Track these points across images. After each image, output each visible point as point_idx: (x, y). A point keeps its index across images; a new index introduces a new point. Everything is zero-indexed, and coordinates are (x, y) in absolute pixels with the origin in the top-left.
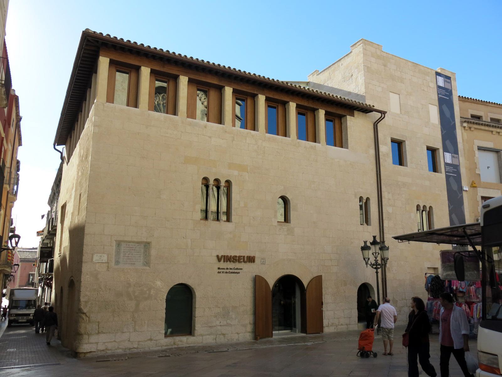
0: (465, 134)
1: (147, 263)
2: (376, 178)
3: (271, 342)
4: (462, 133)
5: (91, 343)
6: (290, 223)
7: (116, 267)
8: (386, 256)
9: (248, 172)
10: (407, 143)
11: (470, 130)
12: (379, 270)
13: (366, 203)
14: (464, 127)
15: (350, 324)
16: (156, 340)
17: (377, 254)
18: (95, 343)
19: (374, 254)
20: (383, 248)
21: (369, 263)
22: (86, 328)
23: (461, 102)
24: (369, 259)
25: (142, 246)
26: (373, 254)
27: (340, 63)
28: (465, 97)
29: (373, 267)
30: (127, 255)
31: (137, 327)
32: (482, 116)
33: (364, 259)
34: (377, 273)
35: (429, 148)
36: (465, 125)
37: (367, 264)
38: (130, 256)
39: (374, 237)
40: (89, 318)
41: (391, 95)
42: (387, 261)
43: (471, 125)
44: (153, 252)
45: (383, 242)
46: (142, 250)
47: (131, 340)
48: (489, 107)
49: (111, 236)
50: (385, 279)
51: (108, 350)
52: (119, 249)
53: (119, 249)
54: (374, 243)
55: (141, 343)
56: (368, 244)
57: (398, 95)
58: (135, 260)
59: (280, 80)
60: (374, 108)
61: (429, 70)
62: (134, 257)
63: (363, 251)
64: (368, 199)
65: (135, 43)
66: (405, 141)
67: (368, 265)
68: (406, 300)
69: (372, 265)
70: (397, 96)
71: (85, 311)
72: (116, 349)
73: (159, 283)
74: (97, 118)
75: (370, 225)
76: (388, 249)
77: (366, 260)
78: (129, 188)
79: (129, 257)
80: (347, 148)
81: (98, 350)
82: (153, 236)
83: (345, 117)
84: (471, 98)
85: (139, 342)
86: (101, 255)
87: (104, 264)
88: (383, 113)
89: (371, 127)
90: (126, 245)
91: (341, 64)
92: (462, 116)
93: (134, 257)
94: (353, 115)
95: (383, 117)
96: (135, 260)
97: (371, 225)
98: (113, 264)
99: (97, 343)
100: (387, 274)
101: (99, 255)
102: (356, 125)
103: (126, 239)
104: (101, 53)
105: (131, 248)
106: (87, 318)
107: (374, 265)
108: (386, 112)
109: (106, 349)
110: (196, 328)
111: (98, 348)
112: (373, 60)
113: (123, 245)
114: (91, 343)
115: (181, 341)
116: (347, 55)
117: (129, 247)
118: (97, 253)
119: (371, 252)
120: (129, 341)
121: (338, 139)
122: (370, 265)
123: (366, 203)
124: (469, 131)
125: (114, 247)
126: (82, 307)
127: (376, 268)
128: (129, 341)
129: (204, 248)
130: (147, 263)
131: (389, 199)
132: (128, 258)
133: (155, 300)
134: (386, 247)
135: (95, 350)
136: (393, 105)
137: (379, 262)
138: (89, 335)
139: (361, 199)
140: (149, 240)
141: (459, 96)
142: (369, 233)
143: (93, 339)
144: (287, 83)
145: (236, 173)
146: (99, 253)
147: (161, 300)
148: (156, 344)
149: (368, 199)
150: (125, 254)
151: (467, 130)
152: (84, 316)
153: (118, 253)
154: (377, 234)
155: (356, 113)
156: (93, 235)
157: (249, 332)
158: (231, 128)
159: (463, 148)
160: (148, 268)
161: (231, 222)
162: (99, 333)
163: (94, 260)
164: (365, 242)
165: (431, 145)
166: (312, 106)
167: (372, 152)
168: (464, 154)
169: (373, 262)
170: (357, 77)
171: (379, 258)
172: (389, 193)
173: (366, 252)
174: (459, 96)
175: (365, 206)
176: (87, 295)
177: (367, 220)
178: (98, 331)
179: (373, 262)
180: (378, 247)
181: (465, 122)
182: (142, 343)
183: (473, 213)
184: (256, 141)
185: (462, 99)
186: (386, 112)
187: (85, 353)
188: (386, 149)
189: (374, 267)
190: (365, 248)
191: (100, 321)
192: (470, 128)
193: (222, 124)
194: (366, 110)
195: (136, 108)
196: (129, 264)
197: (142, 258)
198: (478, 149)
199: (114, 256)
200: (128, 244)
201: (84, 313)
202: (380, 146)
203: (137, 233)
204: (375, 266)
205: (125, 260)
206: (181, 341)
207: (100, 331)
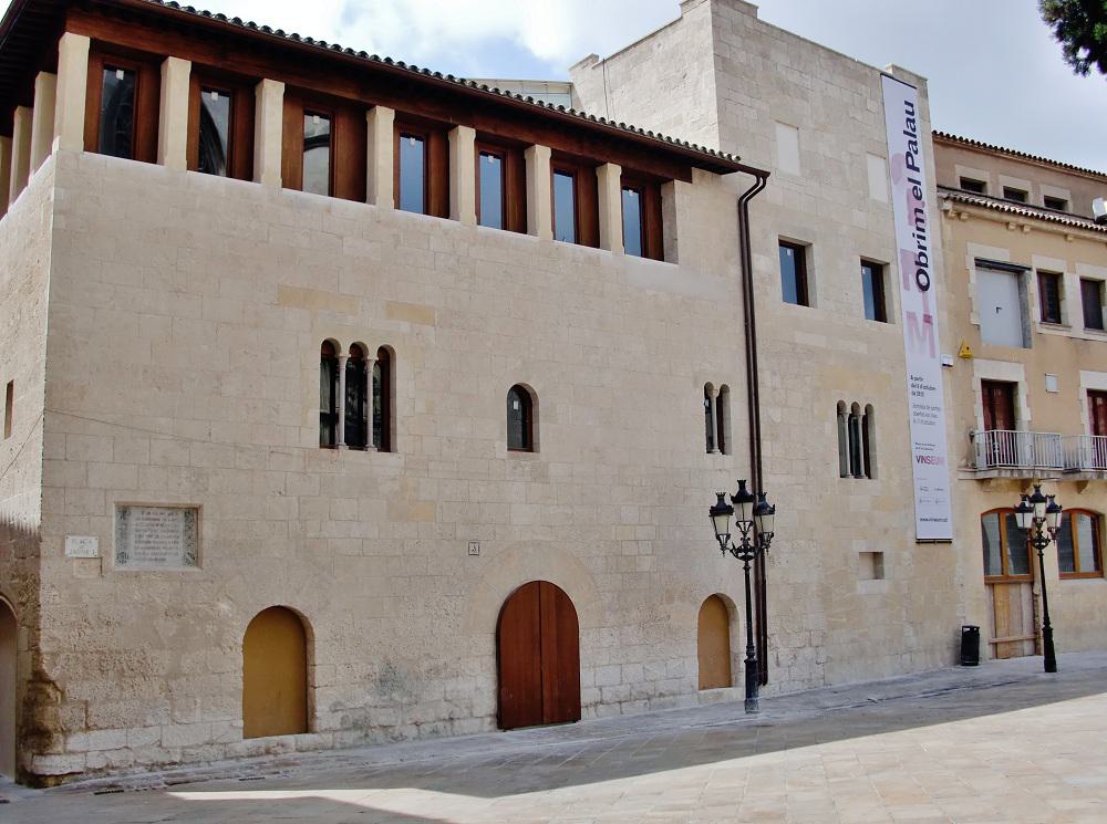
0: (948, 227)
1: (194, 558)
2: (743, 336)
3: (578, 734)
4: (941, 225)
5: (73, 753)
6: (539, 452)
7: (123, 568)
8: (768, 528)
9: (434, 325)
10: (815, 247)
11: (959, 218)
12: (751, 563)
13: (720, 400)
14: (946, 212)
15: (680, 694)
16: (225, 744)
17: (747, 524)
18: (82, 752)
19: (741, 524)
20: (762, 509)
21: (730, 546)
22: (56, 717)
23: (939, 147)
24: (728, 536)
25: (181, 515)
26: (737, 524)
27: (654, 43)
28: (948, 135)
29: (737, 557)
30: (145, 539)
31: (177, 713)
32: (985, 183)
33: (718, 537)
34: (747, 568)
35: (865, 263)
36: (948, 205)
37: (723, 548)
38: (151, 539)
39: (742, 484)
40: (63, 693)
41: (780, 129)
42: (769, 541)
43: (960, 208)
44: (207, 529)
45: (762, 496)
46: (182, 526)
47: (164, 745)
48: (1001, 160)
49: (106, 490)
50: (764, 582)
51: (113, 768)
52: (126, 525)
53: (126, 525)
54: (741, 498)
55: (188, 750)
56: (728, 501)
57: (795, 131)
58: (164, 551)
59: (458, 76)
60: (740, 162)
61: (867, 70)
62: (162, 542)
63: (716, 518)
64: (724, 389)
65: (222, 16)
66: (811, 244)
67: (727, 552)
68: (810, 631)
69: (736, 551)
70: (792, 133)
71: (53, 674)
72: (130, 766)
73: (224, 606)
74: (62, 191)
75: (730, 454)
76: (772, 511)
77: (722, 540)
78: (145, 371)
79: (149, 542)
80: (674, 261)
81: (89, 769)
82: (207, 489)
83: (669, 184)
84: (961, 138)
85: (183, 748)
86: (82, 538)
87: (93, 562)
88: (762, 175)
89: (733, 208)
90: (143, 513)
91: (656, 44)
92: (940, 184)
93: (162, 542)
94: (689, 179)
95: (761, 185)
96: (164, 551)
97: (730, 454)
98: (112, 561)
99: (85, 753)
100: (768, 572)
101: (79, 538)
102: (694, 207)
103: (142, 498)
104: (70, 23)
105: (155, 519)
106: (58, 693)
107: (739, 550)
108: (768, 174)
109: (107, 766)
110: (318, 714)
111: (88, 765)
112: (736, 41)
113: (135, 515)
114: (73, 753)
115: (283, 746)
116: (671, 25)
117: (147, 519)
118: (74, 534)
119: (733, 519)
120: (160, 746)
121: (653, 242)
122: (731, 551)
123: (720, 400)
124: (957, 222)
125: (114, 520)
126: (44, 667)
127: (746, 558)
128: (160, 746)
129: (330, 519)
130: (194, 558)
131: (775, 389)
132: (148, 545)
133: (218, 649)
134: (768, 506)
135: (81, 770)
136: (783, 154)
137: (751, 543)
138: (66, 732)
139: (708, 389)
140: (196, 502)
141: (935, 132)
142: (729, 472)
143: (76, 741)
144: (463, 80)
145: (405, 327)
146: (79, 534)
147: (231, 648)
148: (225, 753)
149: (724, 389)
150: (140, 536)
151: (952, 218)
152: (50, 690)
153: (123, 534)
154: (746, 475)
155: (696, 172)
156: (63, 491)
157: (490, 715)
158: (469, 228)
159: (942, 260)
160: (196, 569)
161: (396, 451)
162: (88, 728)
163: (67, 552)
164: (721, 497)
165: (794, 236)
166: (590, 155)
167: (735, 271)
168: (945, 276)
169: (739, 544)
170: (698, 82)
171: (750, 535)
172: (775, 374)
173: (721, 520)
174: (935, 132)
175: (716, 405)
176: (54, 639)
177: (717, 439)
178: (86, 724)
179: (739, 544)
180: (749, 507)
181: (947, 198)
182: (192, 751)
183: (962, 418)
184: (454, 246)
185: (943, 140)
186: (768, 174)
187: (57, 776)
188: (768, 263)
189: (740, 555)
190: (720, 510)
191: (89, 699)
192: (959, 214)
193: (529, 231)
194: (719, 166)
195: (251, 180)
196: (151, 559)
197: (181, 545)
198: (977, 265)
199: (113, 544)
200: (147, 510)
201: (50, 682)
202: (754, 256)
203: (167, 484)
204: (742, 552)
205: (139, 551)
206: (283, 746)
207: (91, 724)
